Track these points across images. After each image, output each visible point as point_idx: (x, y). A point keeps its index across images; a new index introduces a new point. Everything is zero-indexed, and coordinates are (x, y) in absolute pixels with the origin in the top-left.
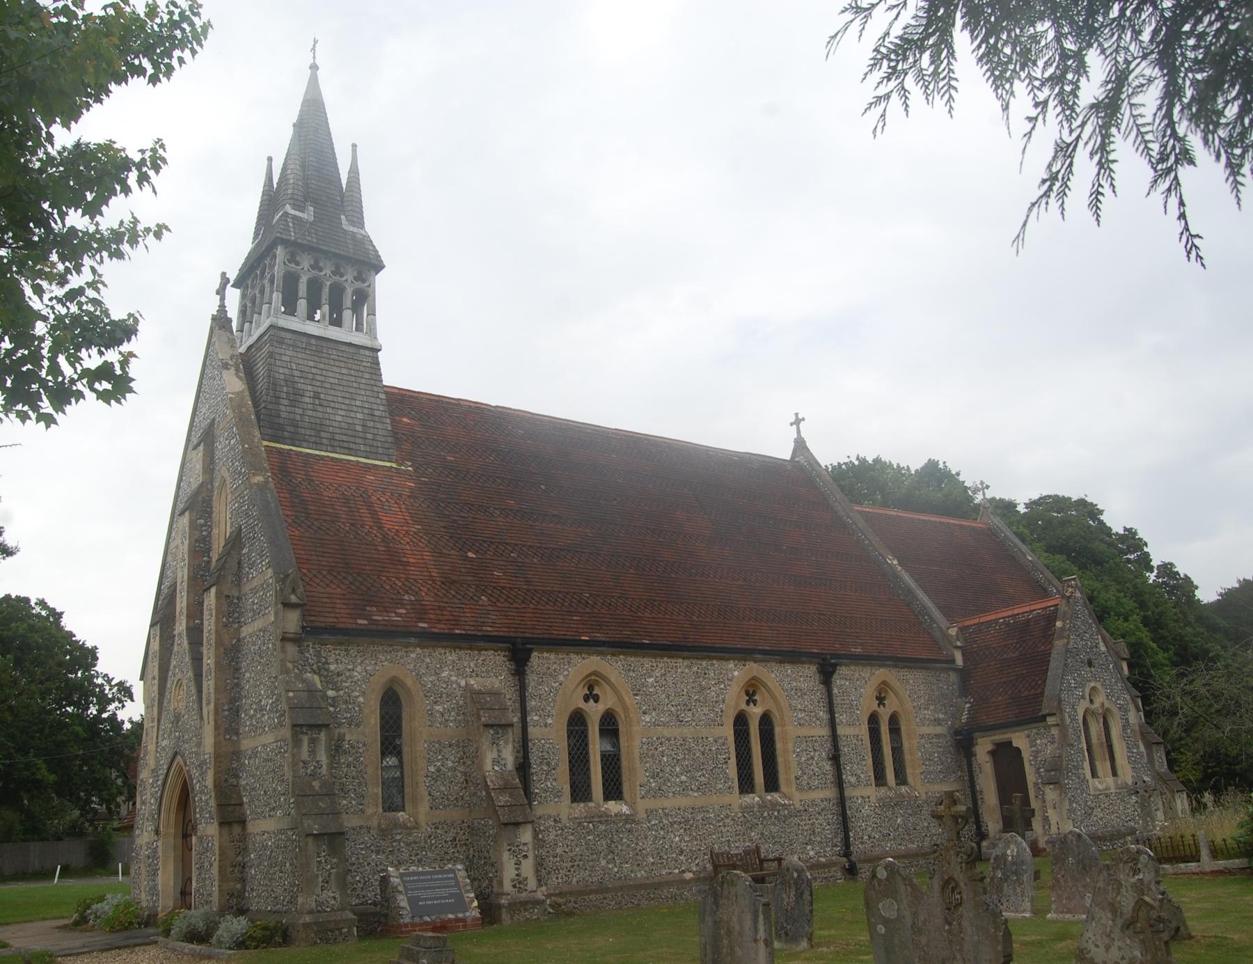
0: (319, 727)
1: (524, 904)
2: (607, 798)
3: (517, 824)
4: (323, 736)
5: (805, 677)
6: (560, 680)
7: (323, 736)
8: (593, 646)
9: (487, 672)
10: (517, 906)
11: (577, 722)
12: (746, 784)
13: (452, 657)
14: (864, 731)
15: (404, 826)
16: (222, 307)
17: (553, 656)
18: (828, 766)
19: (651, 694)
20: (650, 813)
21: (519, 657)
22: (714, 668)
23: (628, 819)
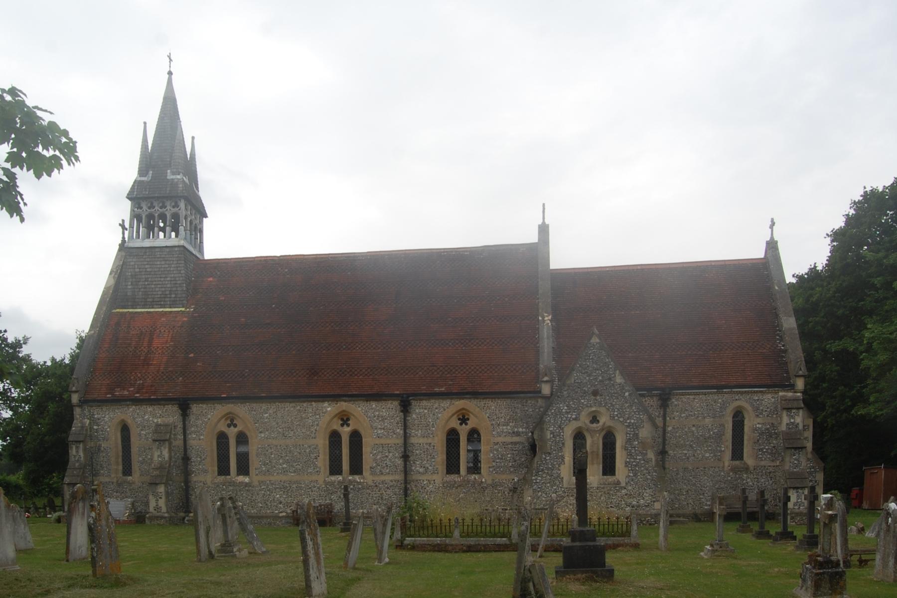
0: (80, 442)
1: (157, 518)
2: (239, 474)
3: (157, 484)
4: (81, 445)
5: (389, 410)
6: (208, 419)
7: (81, 445)
8: (229, 399)
9: (169, 415)
10: (152, 518)
11: (222, 438)
13: (150, 409)
14: (439, 442)
15: (129, 483)
16: (124, 238)
17: (204, 406)
18: (400, 462)
19: (266, 423)
20: (261, 483)
21: (184, 407)
22: (311, 407)
23: (246, 485)
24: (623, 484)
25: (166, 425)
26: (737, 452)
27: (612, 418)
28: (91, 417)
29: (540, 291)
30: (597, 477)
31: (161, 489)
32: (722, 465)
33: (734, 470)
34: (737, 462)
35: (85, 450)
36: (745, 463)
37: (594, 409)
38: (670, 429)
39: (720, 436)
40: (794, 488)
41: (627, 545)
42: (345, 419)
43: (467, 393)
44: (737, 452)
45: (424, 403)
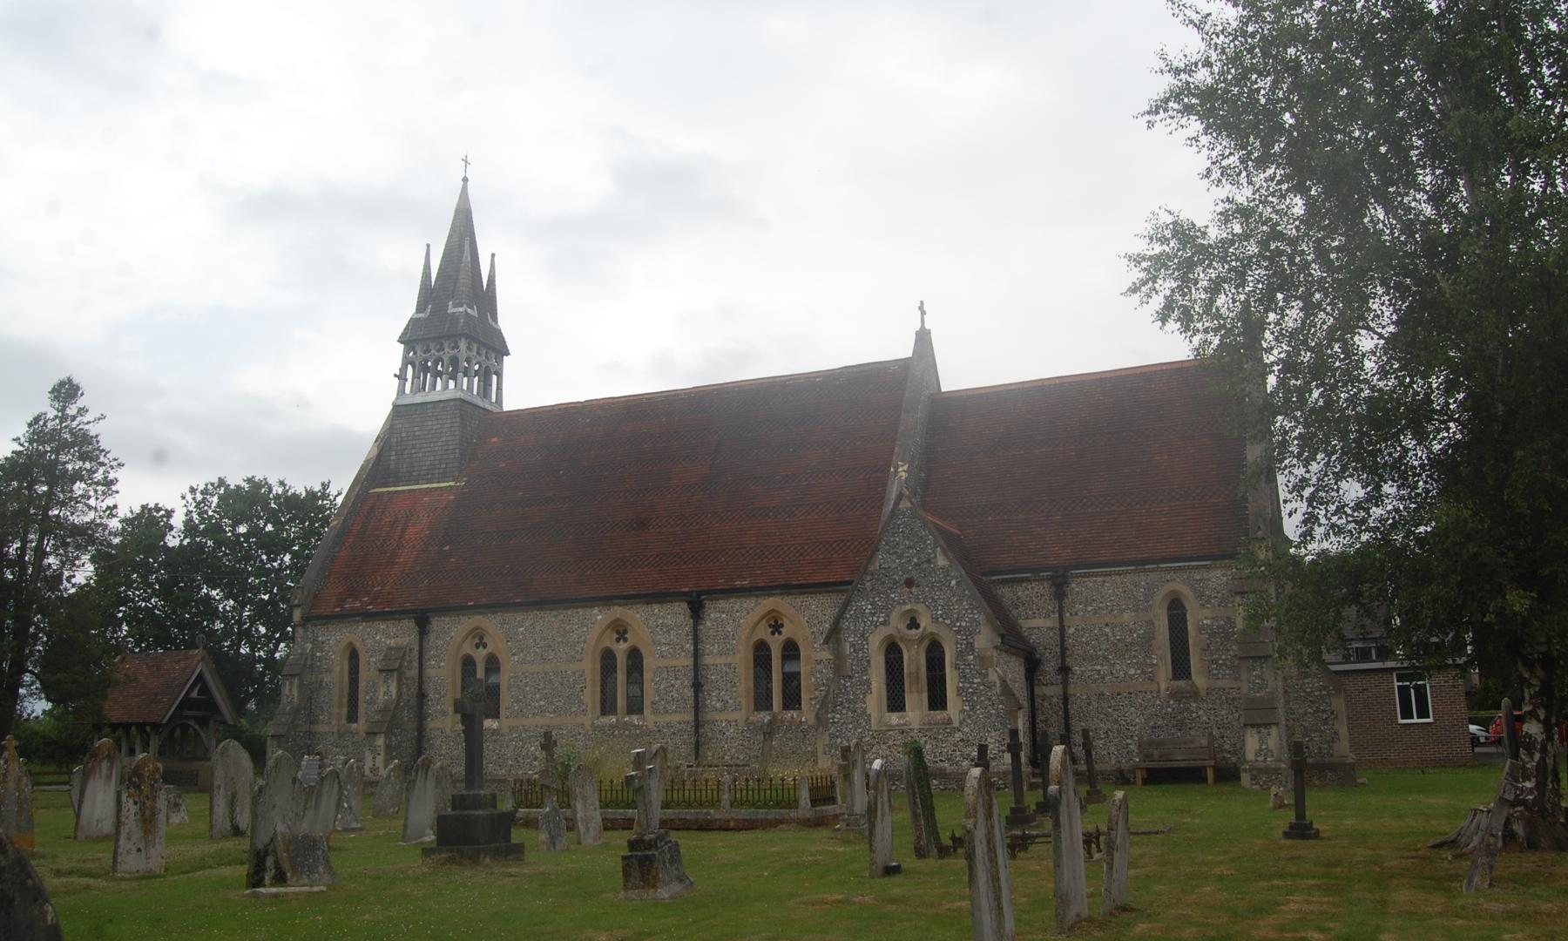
2: (630, 711)
3: (375, 734)
5: (675, 614)
8: (477, 609)
12: (607, 707)
14: (742, 660)
18: (689, 693)
20: (512, 728)
24: (956, 724)
25: (398, 648)
26: (1181, 668)
27: (935, 619)
28: (315, 643)
29: (901, 429)
30: (918, 713)
31: (380, 741)
32: (1155, 688)
33: (1175, 695)
34: (1181, 683)
35: (300, 686)
36: (1193, 685)
37: (908, 607)
38: (1071, 631)
39: (1147, 641)
40: (1252, 726)
41: (793, 821)
42: (621, 631)
43: (776, 587)
44: (1181, 668)
45: (722, 604)
